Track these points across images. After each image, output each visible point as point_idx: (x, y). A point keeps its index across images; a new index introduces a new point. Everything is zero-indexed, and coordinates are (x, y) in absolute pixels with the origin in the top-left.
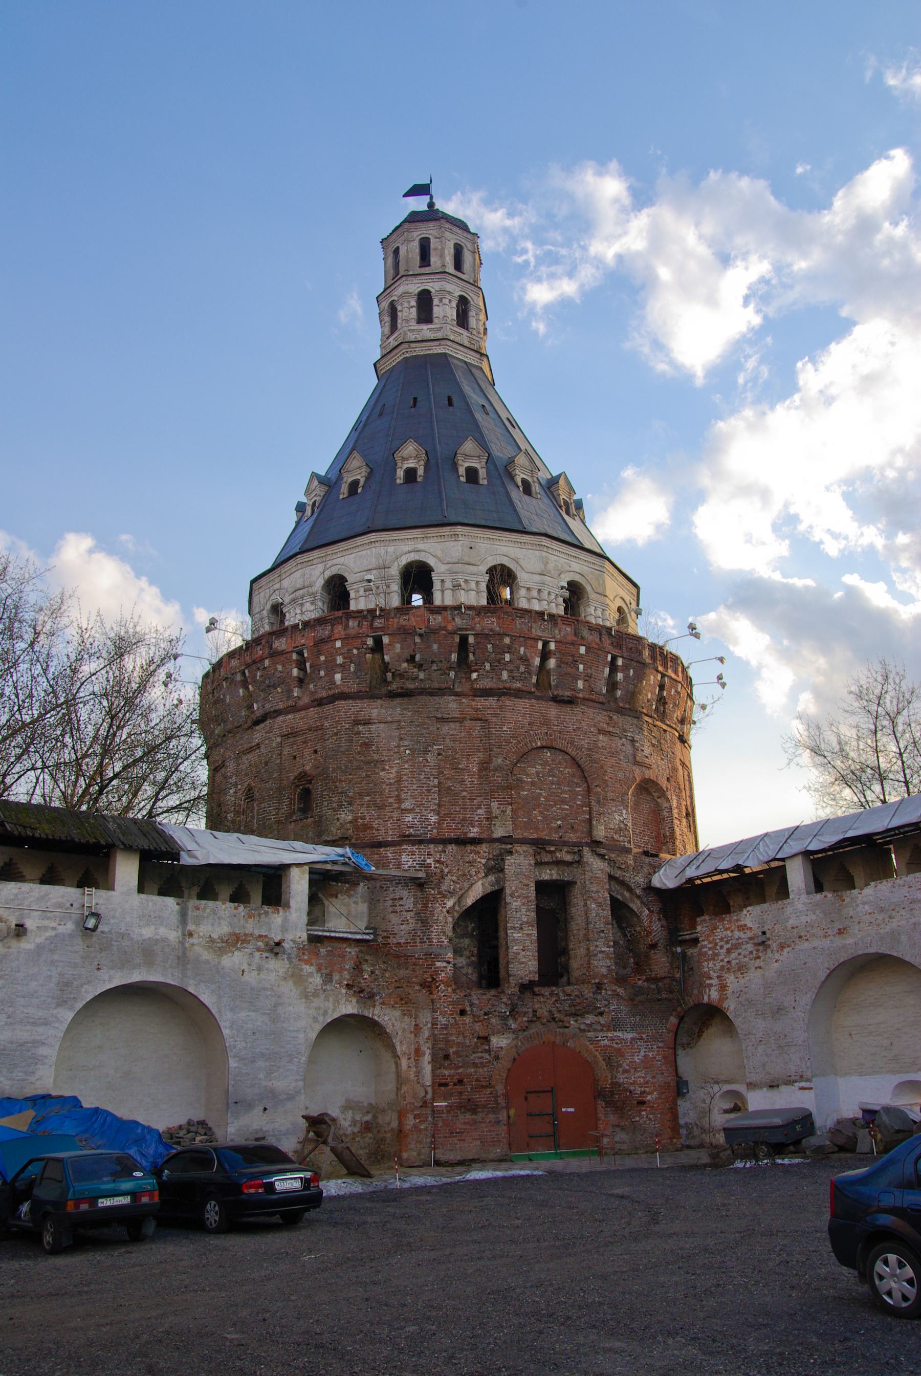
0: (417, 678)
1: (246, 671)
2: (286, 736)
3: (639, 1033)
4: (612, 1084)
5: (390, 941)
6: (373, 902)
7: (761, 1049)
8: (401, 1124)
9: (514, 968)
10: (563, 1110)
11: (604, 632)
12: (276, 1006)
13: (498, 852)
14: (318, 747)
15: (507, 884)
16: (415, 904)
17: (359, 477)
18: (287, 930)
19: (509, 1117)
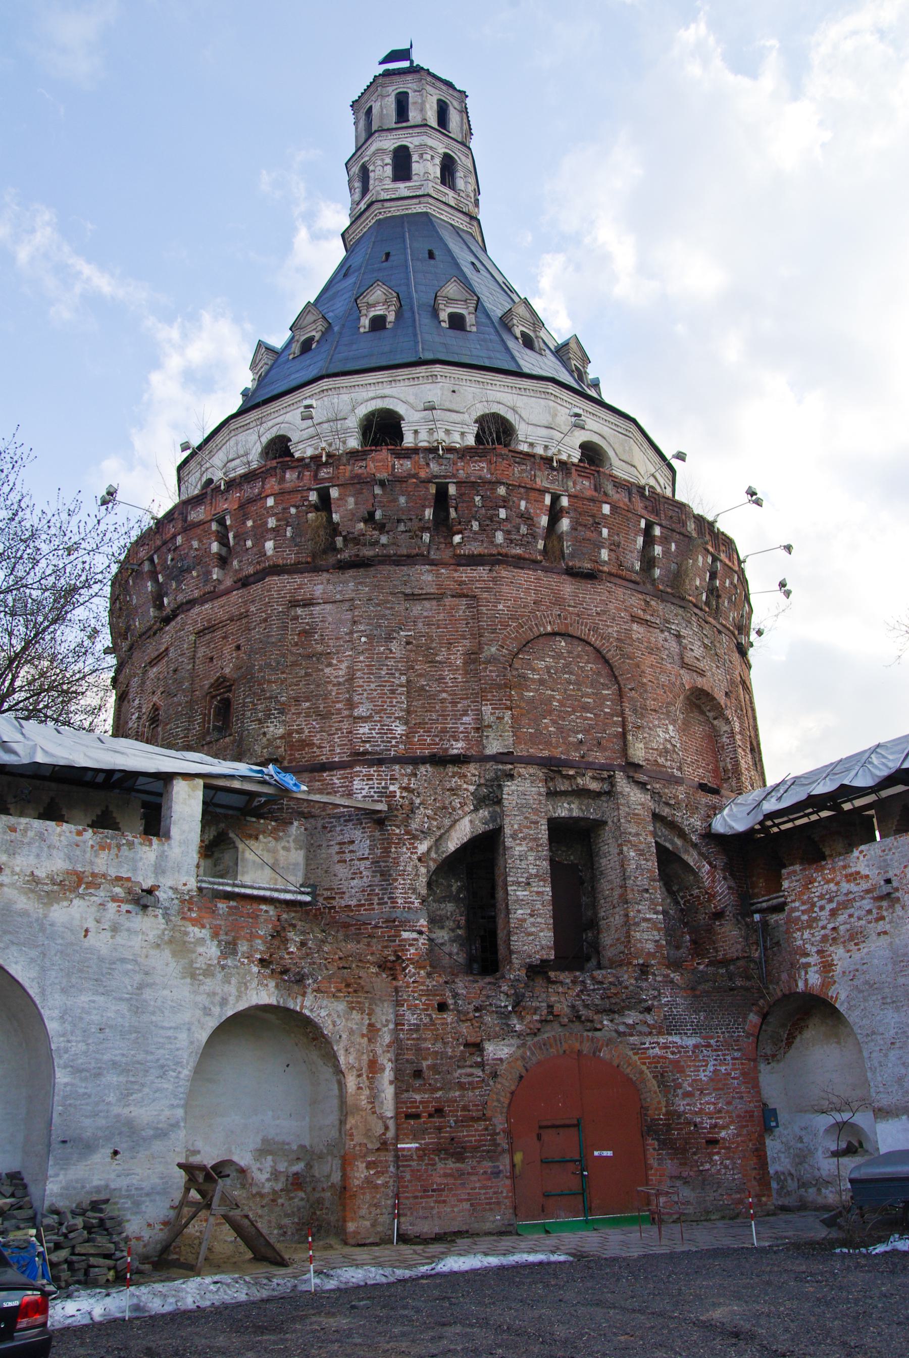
0: (377, 542)
1: (155, 557)
2: (200, 633)
3: (703, 1038)
4: (668, 1113)
5: (334, 903)
6: (312, 849)
7: (893, 1055)
8: (345, 1177)
9: (518, 942)
10: (596, 1153)
11: (634, 490)
12: (141, 987)
13: (492, 774)
14: (242, 642)
15: (507, 820)
16: (372, 848)
17: (313, 333)
18: (164, 872)
19: (513, 1166)
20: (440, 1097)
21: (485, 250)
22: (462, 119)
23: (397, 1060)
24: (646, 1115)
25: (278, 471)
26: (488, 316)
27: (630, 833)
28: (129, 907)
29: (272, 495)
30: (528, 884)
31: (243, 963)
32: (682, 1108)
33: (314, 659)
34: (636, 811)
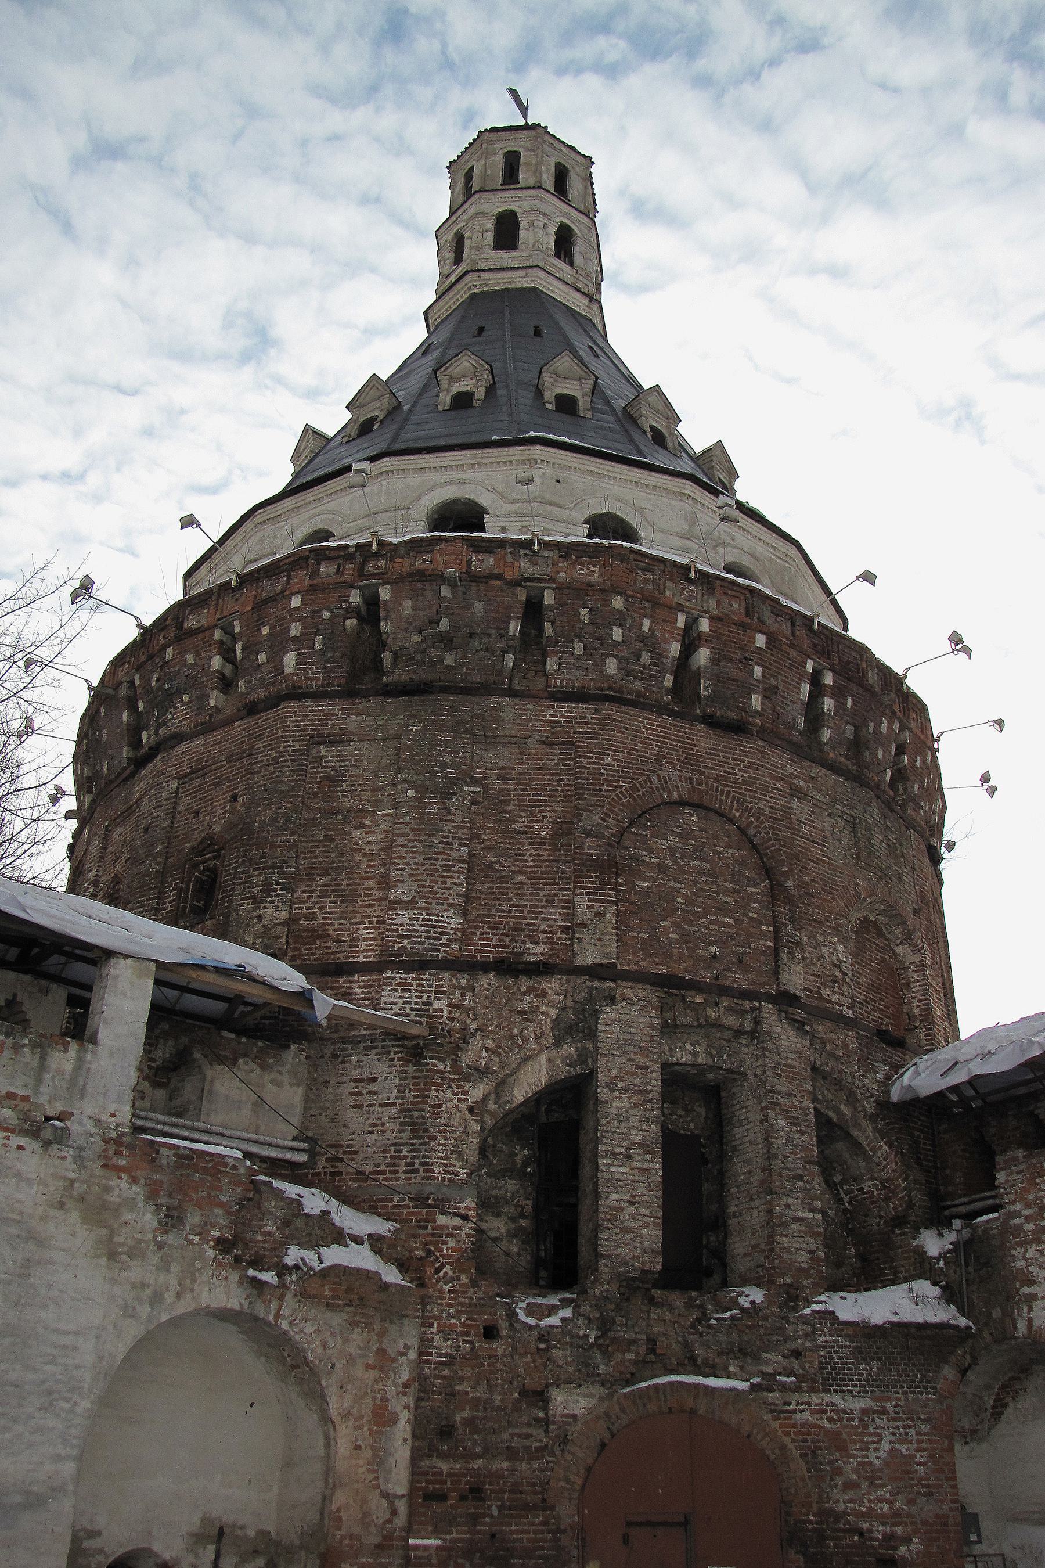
6: (314, 1088)
9: (609, 1241)
15: (602, 1061)
20: (479, 1469)
21: (605, 338)
22: (586, 188)
23: (417, 1408)
24: (788, 1514)
25: (310, 562)
26: (607, 402)
27: (779, 1093)
28: (23, 1141)
29: (299, 592)
30: (629, 1157)
31: (191, 1242)
32: (842, 1506)
33: (339, 817)
34: (789, 1061)
